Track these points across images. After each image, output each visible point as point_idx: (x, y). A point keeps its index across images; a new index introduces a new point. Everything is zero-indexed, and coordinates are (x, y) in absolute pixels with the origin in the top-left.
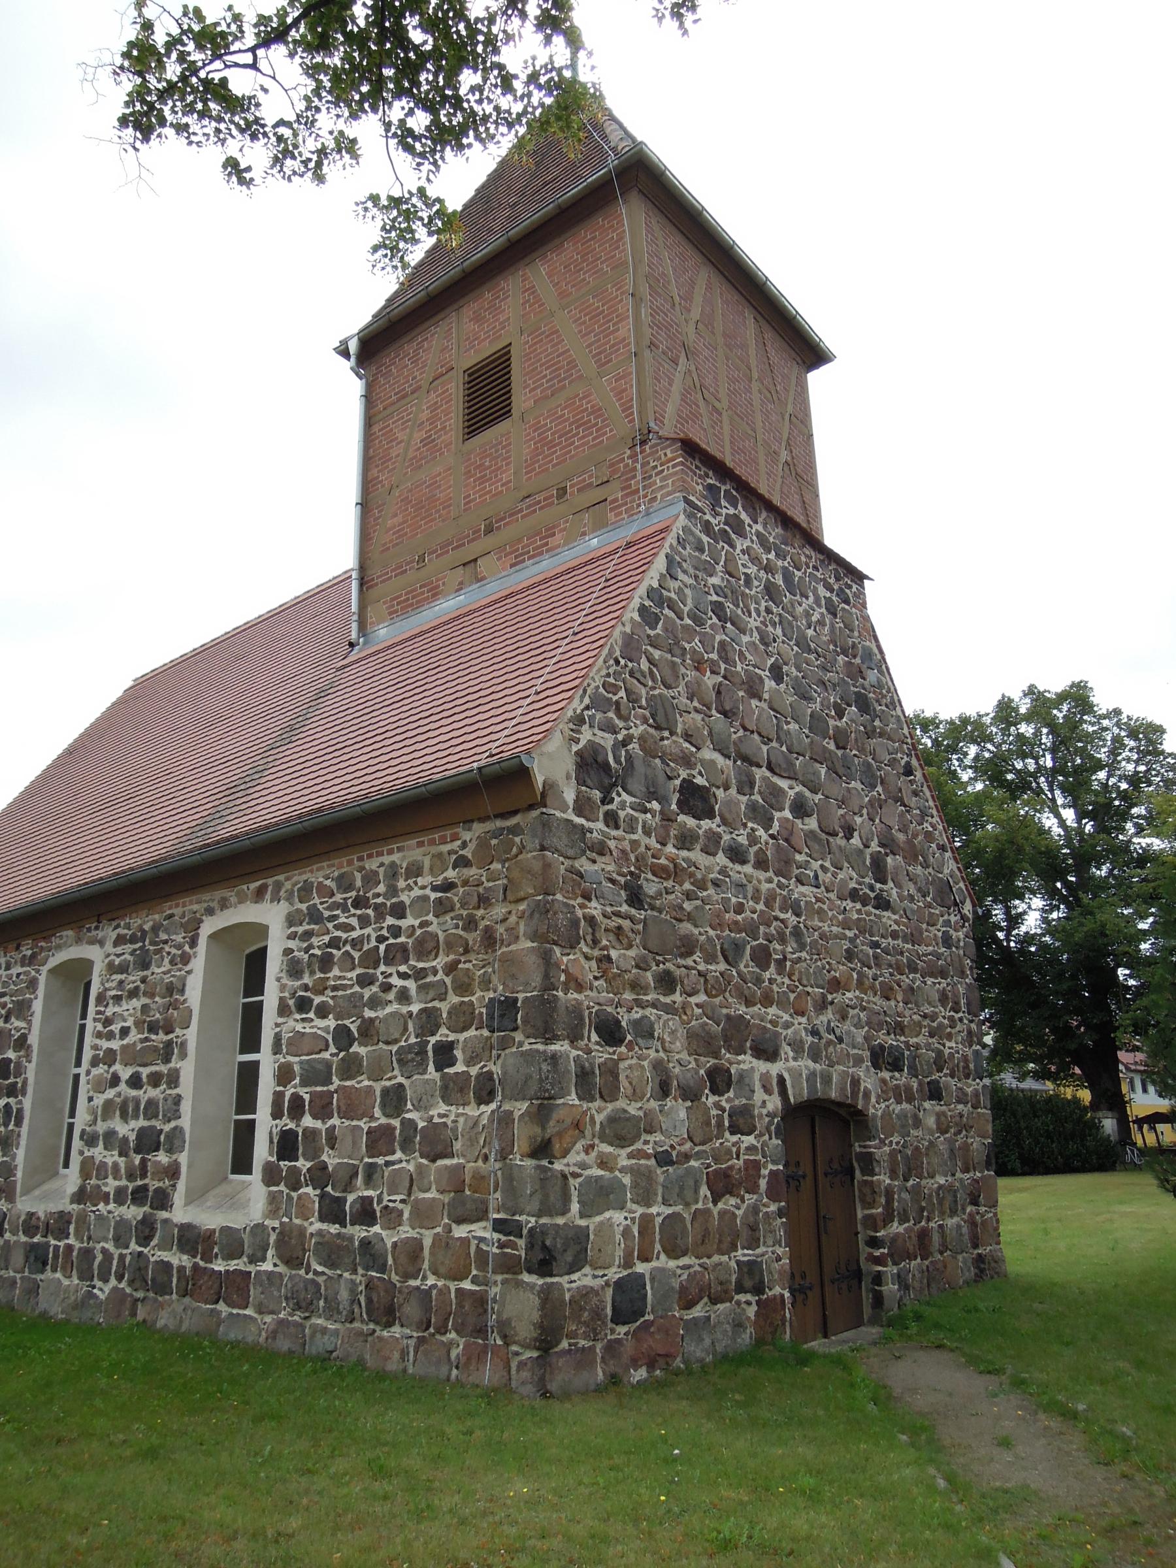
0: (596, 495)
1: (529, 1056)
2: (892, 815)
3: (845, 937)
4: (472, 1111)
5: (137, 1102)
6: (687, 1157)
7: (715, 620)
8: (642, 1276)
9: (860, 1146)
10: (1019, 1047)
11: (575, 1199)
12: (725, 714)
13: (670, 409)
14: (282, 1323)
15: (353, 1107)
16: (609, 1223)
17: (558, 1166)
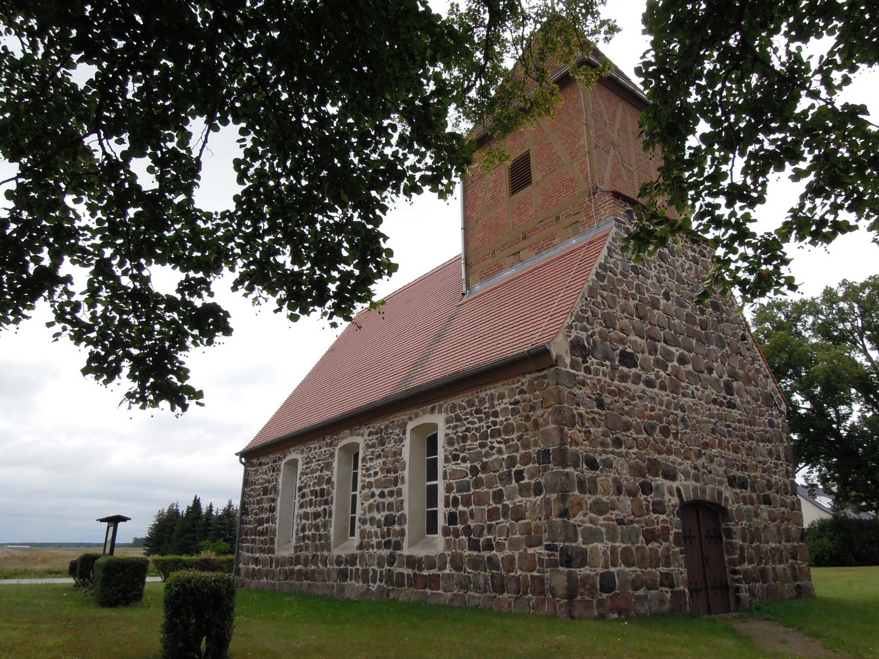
0: (573, 219)
1: (556, 474)
2: (735, 361)
3: (710, 422)
4: (533, 499)
5: (384, 504)
6: (632, 522)
7: (633, 274)
8: (613, 573)
10: (853, 493)
11: (580, 536)
12: (640, 318)
13: (607, 175)
14: (455, 595)
15: (481, 500)
16: (596, 548)
17: (572, 521)
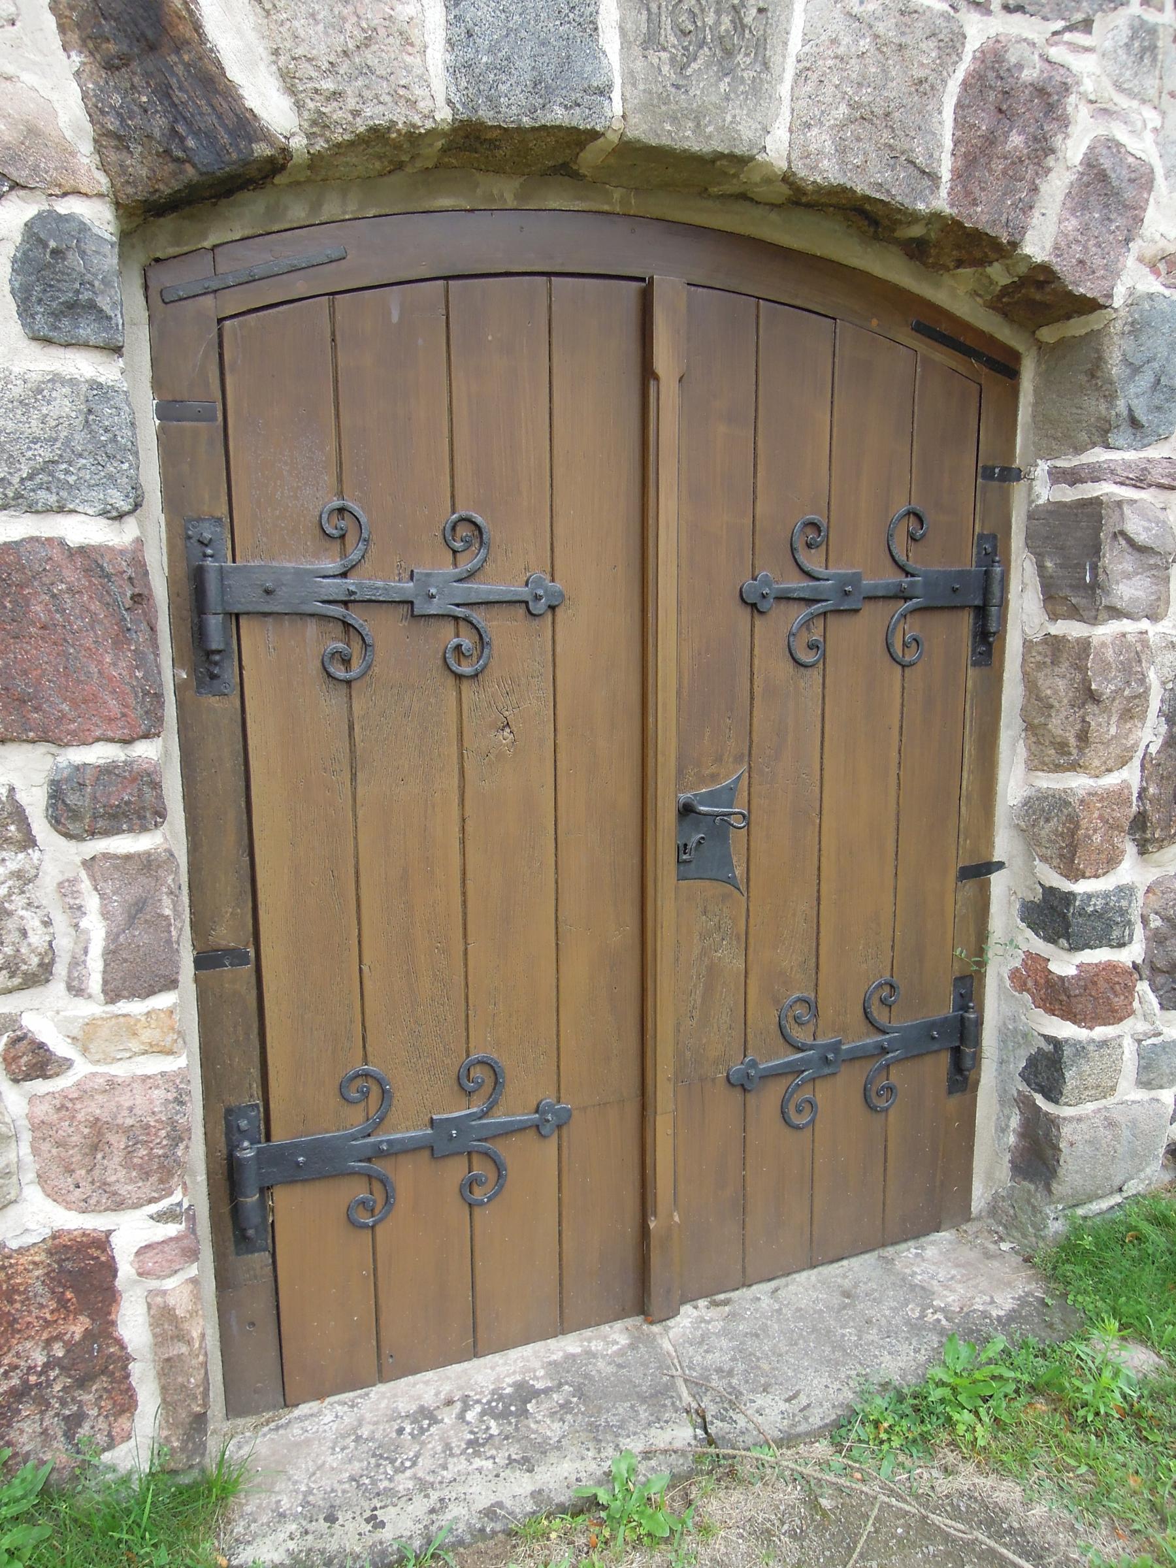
9: (1059, 476)
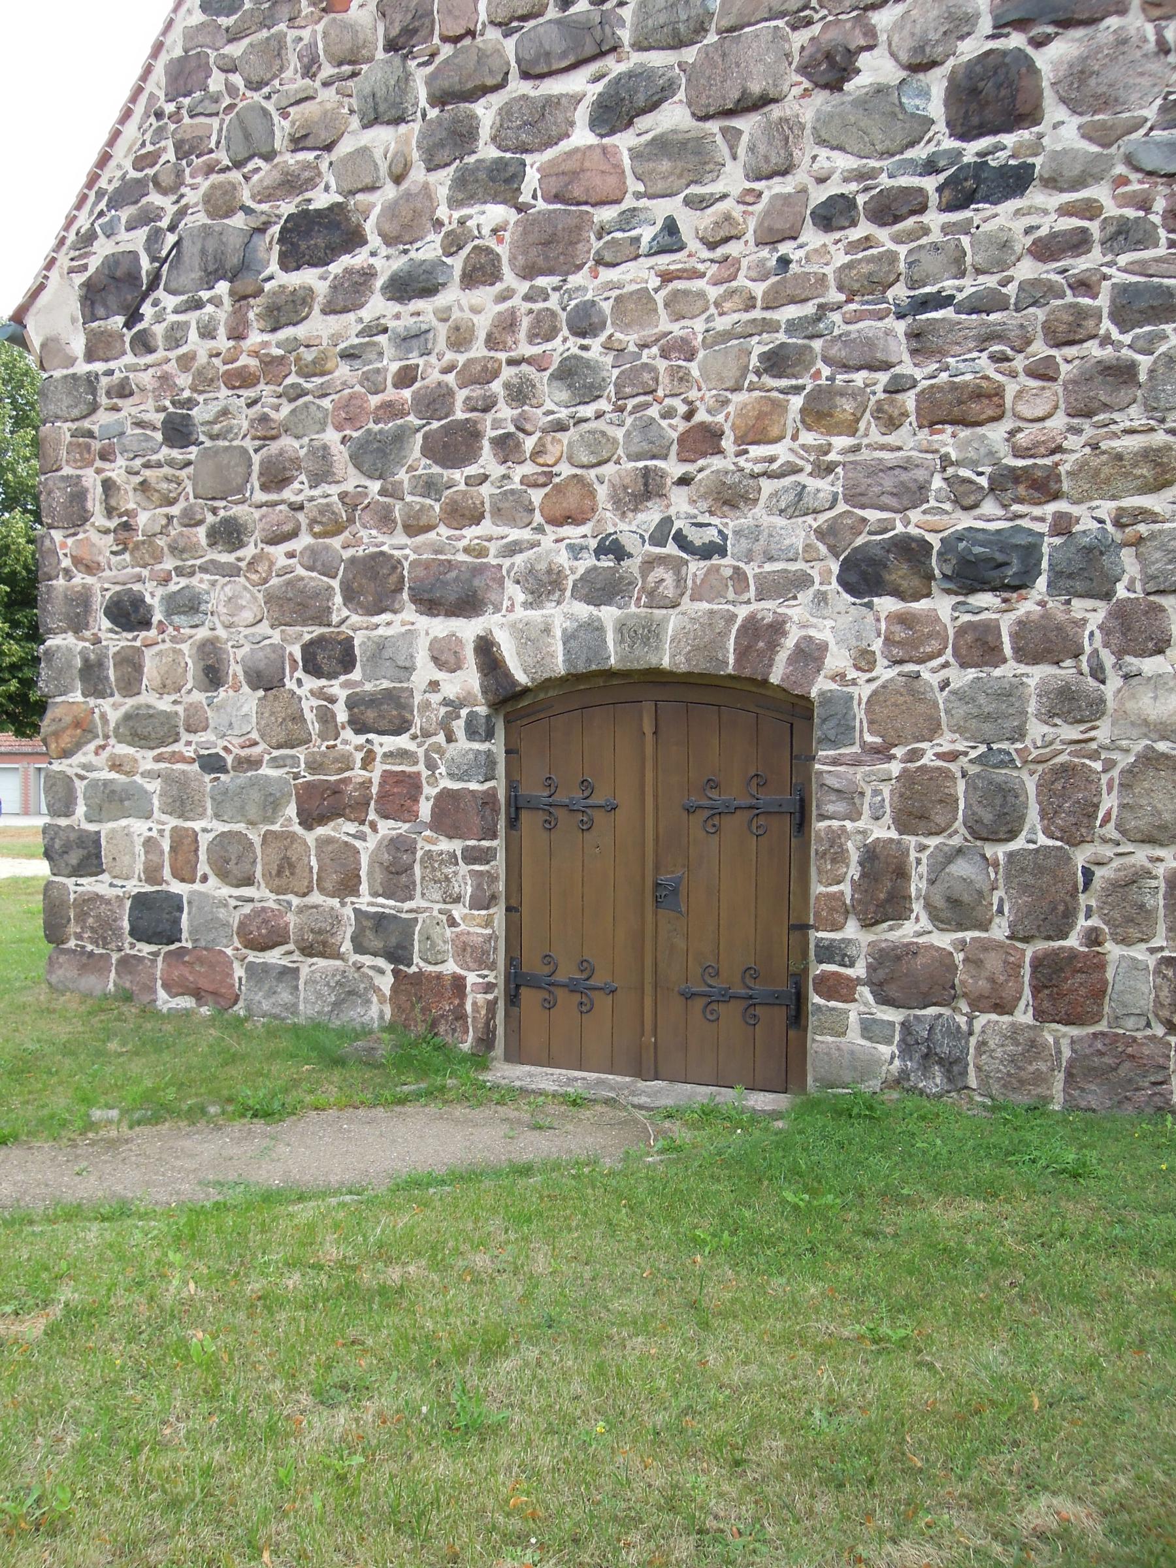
8: (180, 897)
